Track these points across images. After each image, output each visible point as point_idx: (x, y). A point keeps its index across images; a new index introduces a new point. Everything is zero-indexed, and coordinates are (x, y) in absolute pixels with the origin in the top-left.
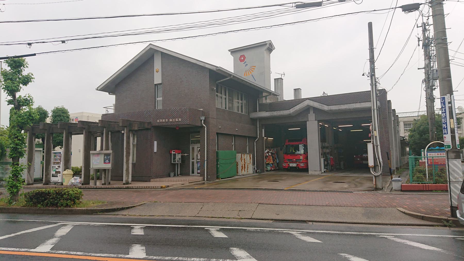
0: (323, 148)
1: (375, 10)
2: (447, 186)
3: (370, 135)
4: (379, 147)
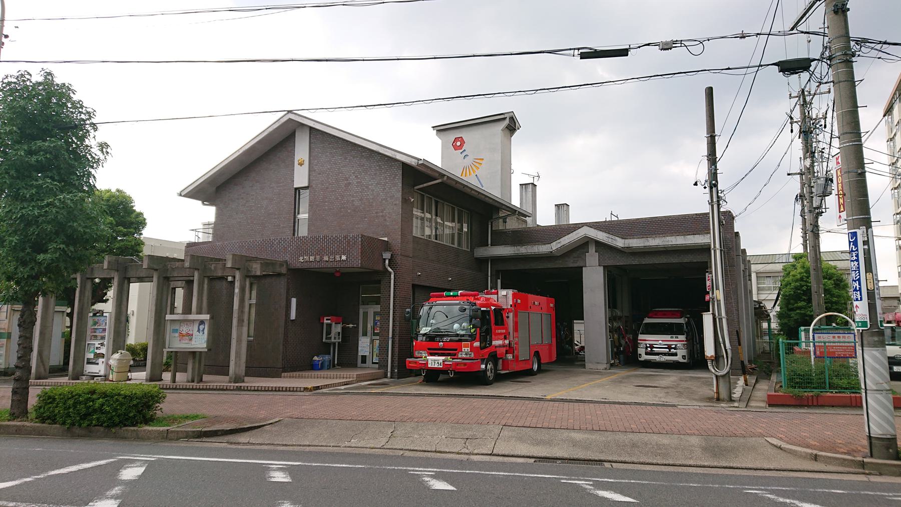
0: (612, 319)
1: (729, 69)
2: (861, 397)
3: (707, 298)
4: (724, 321)
